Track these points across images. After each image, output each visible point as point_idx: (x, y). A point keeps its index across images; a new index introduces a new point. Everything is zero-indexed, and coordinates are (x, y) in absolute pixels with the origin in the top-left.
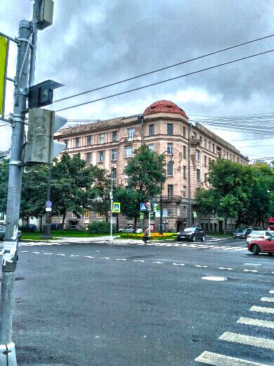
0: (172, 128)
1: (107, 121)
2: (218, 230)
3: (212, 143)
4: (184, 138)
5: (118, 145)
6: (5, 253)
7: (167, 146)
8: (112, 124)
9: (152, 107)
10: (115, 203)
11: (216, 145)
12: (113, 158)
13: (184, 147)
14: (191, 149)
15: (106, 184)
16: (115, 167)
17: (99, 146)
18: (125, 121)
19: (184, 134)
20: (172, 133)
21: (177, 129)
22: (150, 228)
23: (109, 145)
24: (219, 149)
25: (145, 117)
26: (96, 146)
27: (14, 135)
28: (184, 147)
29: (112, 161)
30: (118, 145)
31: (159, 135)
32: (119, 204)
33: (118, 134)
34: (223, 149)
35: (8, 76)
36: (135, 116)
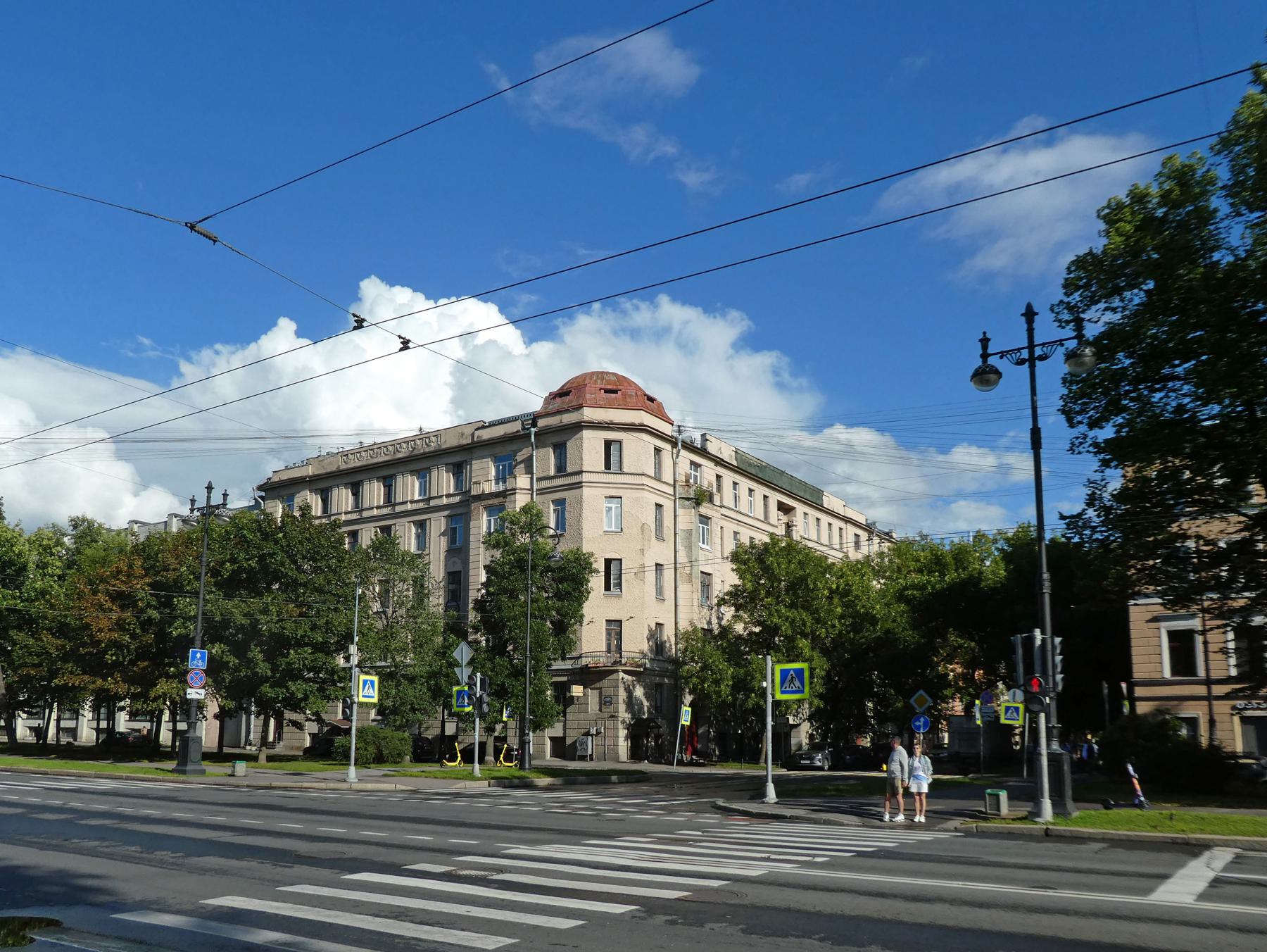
1: (437, 434)
3: (760, 490)
4: (658, 478)
6: (643, 566)
8: (452, 442)
9: (562, 393)
10: (363, 677)
11: (775, 497)
13: (659, 506)
14: (680, 512)
18: (486, 434)
19: (658, 465)
21: (637, 450)
22: (383, 664)
24: (784, 509)
25: (541, 423)
27: (345, 454)
28: (659, 506)
31: (643, 485)
34: (800, 508)
36: (515, 419)
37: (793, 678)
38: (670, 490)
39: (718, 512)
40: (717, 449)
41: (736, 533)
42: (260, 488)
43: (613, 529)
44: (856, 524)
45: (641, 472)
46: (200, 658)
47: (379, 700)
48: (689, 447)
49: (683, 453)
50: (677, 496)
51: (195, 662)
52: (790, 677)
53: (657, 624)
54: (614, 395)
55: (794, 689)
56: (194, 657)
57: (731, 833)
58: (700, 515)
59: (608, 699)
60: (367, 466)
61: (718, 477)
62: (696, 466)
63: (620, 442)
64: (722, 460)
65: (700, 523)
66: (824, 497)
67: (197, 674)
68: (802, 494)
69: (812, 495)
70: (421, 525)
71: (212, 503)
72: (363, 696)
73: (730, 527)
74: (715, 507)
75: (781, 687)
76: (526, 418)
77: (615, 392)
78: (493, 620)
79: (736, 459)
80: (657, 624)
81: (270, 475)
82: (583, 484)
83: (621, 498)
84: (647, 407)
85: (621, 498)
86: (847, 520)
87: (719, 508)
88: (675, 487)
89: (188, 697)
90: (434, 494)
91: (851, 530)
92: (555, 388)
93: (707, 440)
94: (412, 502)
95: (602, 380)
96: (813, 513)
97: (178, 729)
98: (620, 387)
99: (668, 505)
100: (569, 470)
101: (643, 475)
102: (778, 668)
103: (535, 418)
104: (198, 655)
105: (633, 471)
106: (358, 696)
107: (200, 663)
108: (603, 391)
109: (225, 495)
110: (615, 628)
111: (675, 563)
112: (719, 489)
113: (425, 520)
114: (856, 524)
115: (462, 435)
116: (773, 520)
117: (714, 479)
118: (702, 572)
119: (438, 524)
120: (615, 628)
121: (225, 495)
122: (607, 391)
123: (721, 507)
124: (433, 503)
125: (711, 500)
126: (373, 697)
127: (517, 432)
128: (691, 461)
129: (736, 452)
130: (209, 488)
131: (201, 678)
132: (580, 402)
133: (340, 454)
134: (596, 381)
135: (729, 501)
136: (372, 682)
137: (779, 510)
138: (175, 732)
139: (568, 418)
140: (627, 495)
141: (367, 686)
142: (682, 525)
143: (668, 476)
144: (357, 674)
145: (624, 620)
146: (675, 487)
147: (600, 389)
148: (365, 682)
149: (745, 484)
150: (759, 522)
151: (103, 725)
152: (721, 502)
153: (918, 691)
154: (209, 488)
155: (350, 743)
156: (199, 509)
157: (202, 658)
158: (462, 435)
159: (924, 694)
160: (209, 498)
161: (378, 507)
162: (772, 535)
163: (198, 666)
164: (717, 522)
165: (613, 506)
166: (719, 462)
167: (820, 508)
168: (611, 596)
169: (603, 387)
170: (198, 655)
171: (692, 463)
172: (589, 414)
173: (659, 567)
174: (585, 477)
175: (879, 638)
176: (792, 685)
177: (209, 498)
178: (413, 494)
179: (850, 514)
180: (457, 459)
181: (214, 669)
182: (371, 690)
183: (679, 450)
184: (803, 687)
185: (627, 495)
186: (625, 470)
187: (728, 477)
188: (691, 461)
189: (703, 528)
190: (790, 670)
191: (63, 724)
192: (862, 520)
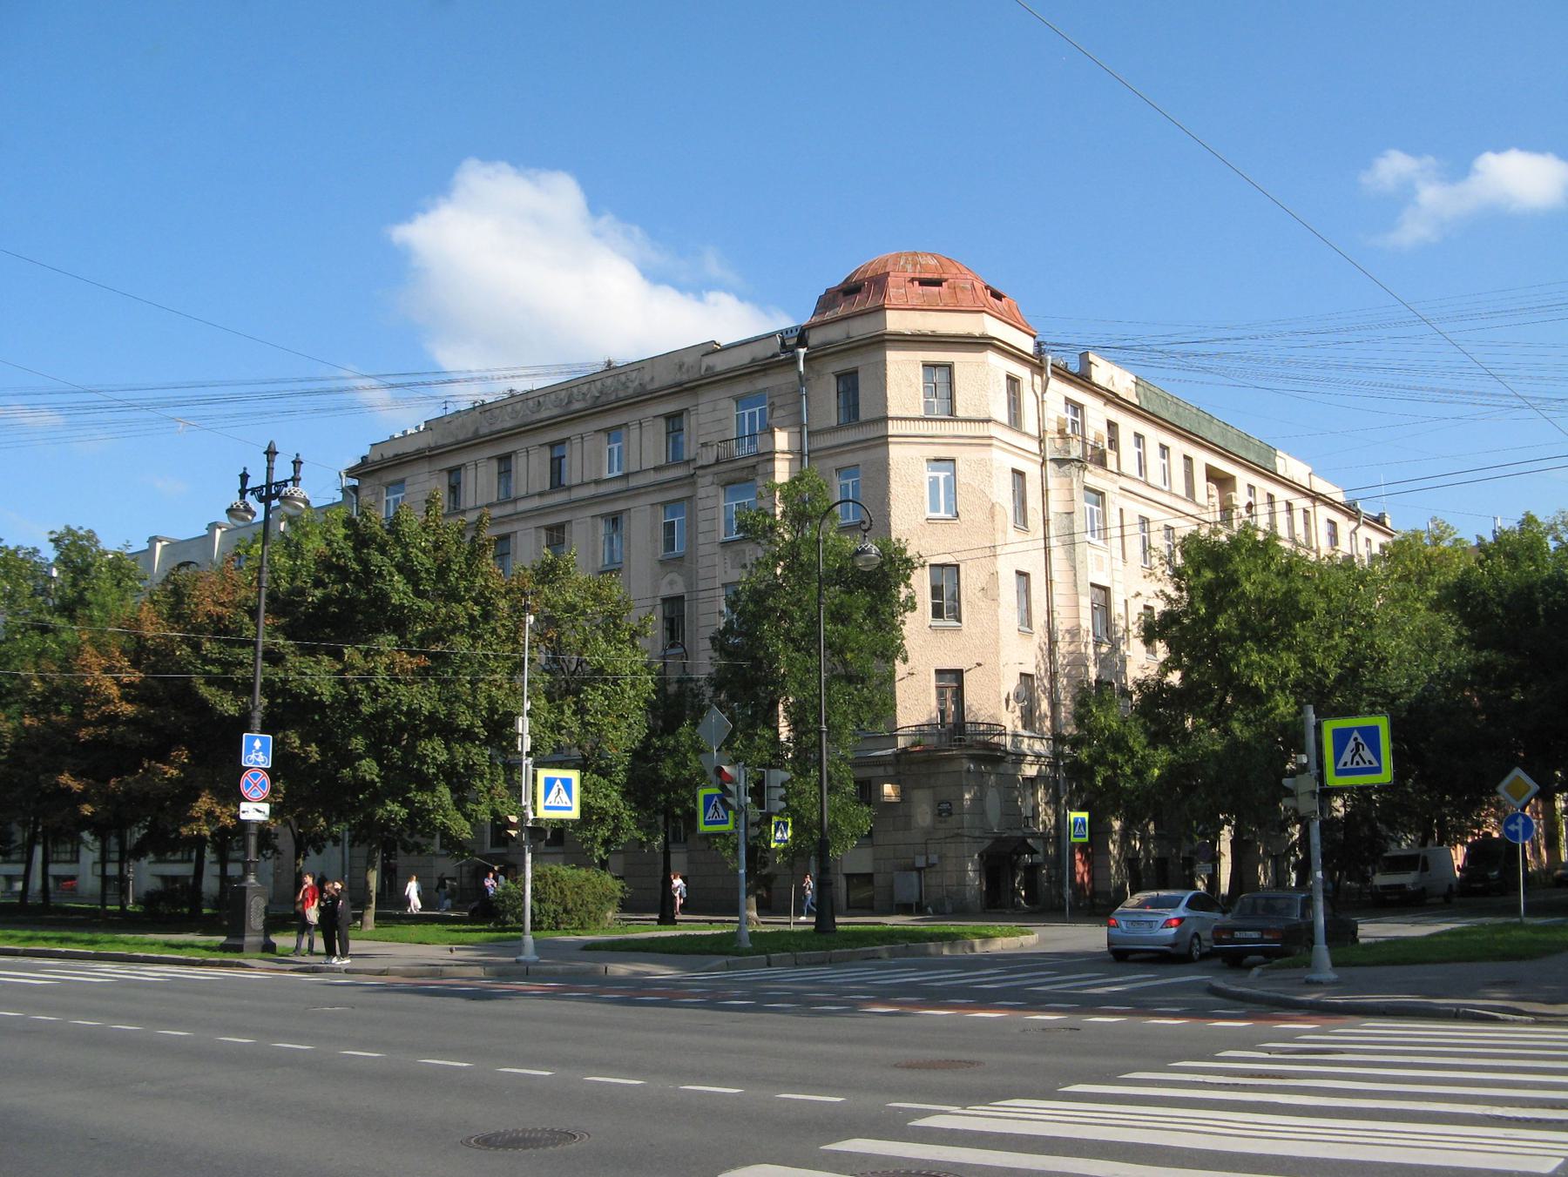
3: (1179, 447)
9: (850, 289)
11: (1202, 458)
25: (815, 338)
28: (1019, 474)
31: (990, 437)
34: (1243, 477)
37: (1358, 745)
39: (1115, 482)
42: (351, 473)
43: (942, 514)
44: (1331, 504)
45: (982, 416)
46: (261, 749)
48: (1063, 374)
49: (1054, 384)
50: (1048, 457)
51: (253, 756)
52: (1352, 744)
53: (1022, 674)
54: (935, 289)
55: (1362, 765)
56: (251, 748)
57: (1341, 1052)
58: (1086, 488)
59: (945, 806)
61: (1112, 426)
62: (1077, 407)
63: (949, 367)
64: (1117, 396)
65: (1086, 501)
66: (1277, 459)
67: (255, 776)
68: (1243, 454)
69: (1259, 456)
70: (615, 520)
71: (276, 478)
73: (1135, 509)
74: (1110, 475)
75: (1337, 761)
76: (790, 335)
77: (937, 283)
79: (1137, 396)
80: (1022, 674)
81: (366, 452)
82: (890, 439)
83: (953, 460)
84: (992, 308)
85: (953, 460)
86: (1315, 497)
87: (1115, 476)
88: (1041, 441)
89: (243, 817)
90: (634, 467)
91: (1323, 513)
92: (837, 281)
93: (1091, 363)
94: (597, 482)
95: (915, 265)
96: (1264, 486)
97: (229, 874)
98: (945, 276)
99: (1032, 470)
100: (863, 416)
101: (988, 421)
102: (1329, 726)
103: (802, 335)
104: (257, 744)
105: (974, 415)
107: (261, 758)
108: (916, 283)
109: (297, 463)
110: (952, 681)
111: (1123, 536)
112: (1114, 443)
113: (621, 512)
114: (1331, 504)
115: (681, 367)
116: (1201, 496)
118: (1093, 585)
119: (643, 523)
120: (952, 681)
121: (297, 463)
122: (924, 282)
123: (1120, 474)
124: (634, 482)
127: (774, 356)
128: (1067, 399)
129: (1136, 383)
130: (271, 453)
131: (263, 785)
132: (881, 302)
133: (478, 410)
134: (904, 267)
137: (1208, 480)
138: (224, 877)
139: (860, 328)
140: (963, 455)
142: (1056, 506)
143: (1030, 423)
144: (530, 767)
146: (1041, 441)
147: (912, 280)
149: (1154, 436)
150: (1178, 501)
151: (113, 869)
152: (1119, 467)
153: (1507, 772)
154: (271, 453)
155: (524, 890)
156: (253, 491)
157: (263, 749)
158: (681, 367)
159: (1524, 776)
160: (270, 470)
161: (541, 494)
162: (1202, 522)
163: (257, 763)
164: (1115, 501)
165: (942, 475)
167: (1272, 476)
168: (943, 629)
169: (917, 276)
170: (257, 744)
171: (1068, 401)
172: (896, 322)
176: (1357, 758)
177: (270, 470)
178: (600, 469)
179: (1320, 486)
180: (671, 407)
181: (282, 767)
182: (564, 795)
184: (1379, 760)
185: (963, 455)
186: (960, 413)
187: (1129, 425)
188: (1067, 399)
189: (1091, 510)
190: (1351, 730)
191: (54, 869)
192: (1340, 497)
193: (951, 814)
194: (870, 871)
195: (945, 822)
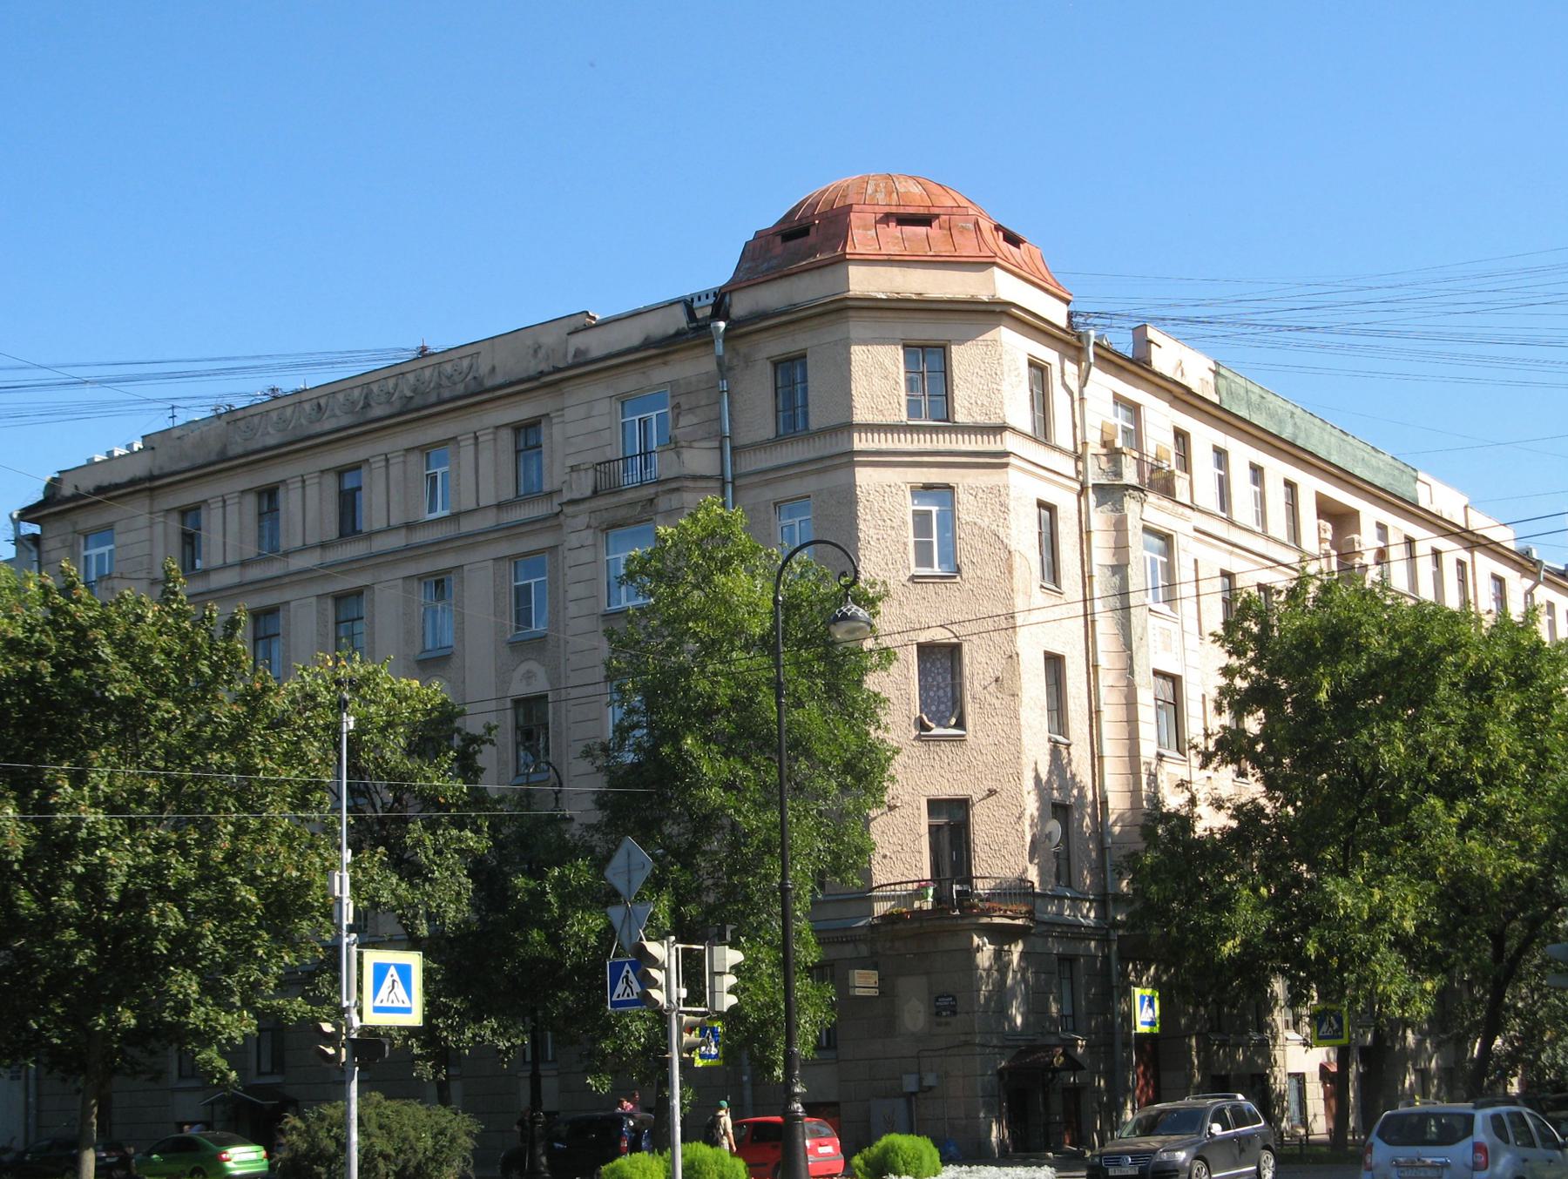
0: (945, 372)
1: (473, 350)
2: (824, 1044)
5: (552, 521)
7: (909, 506)
10: (372, 957)
11: (1310, 486)
12: (523, 618)
15: (261, 751)
16: (540, 685)
17: (420, 537)
18: (596, 344)
20: (948, 415)
23: (487, 521)
25: (741, 305)
26: (396, 541)
29: (514, 645)
30: (552, 521)
32: (414, 960)
33: (553, 436)
34: (1370, 514)
35: (385, 525)
38: (1067, 466)
40: (1175, 362)
41: (1227, 575)
47: (426, 1018)
48: (1112, 361)
59: (944, 1002)
60: (898, 300)
72: (377, 1010)
74: (1181, 509)
77: (925, 220)
78: (98, 1028)
86: (1473, 541)
91: (1485, 565)
93: (1151, 342)
99: (1066, 503)
100: (814, 424)
103: (720, 301)
106: (360, 1013)
113: (448, 571)
116: (1310, 541)
117: (1169, 440)
125: (1167, 490)
126: (408, 1011)
135: (1208, 496)
136: (404, 971)
140: (964, 480)
141: (388, 982)
143: (1062, 434)
144: (354, 949)
145: (975, 798)
148: (381, 971)
161: (323, 546)
166: (1180, 396)
171: (1118, 399)
172: (863, 281)
173: (1055, 663)
174: (860, 442)
175: (1271, 1011)
180: (522, 411)
182: (399, 988)
183: (1090, 364)
186: (961, 417)
193: (954, 1013)
194: (833, 1098)
195: (947, 1024)
